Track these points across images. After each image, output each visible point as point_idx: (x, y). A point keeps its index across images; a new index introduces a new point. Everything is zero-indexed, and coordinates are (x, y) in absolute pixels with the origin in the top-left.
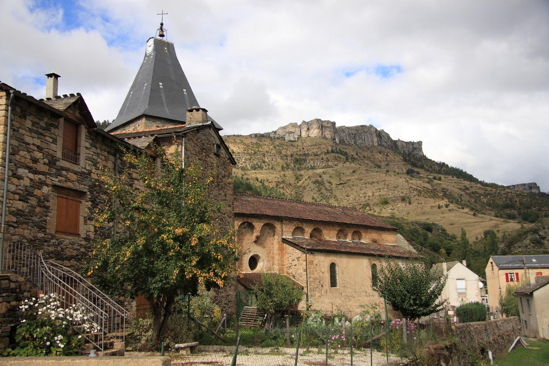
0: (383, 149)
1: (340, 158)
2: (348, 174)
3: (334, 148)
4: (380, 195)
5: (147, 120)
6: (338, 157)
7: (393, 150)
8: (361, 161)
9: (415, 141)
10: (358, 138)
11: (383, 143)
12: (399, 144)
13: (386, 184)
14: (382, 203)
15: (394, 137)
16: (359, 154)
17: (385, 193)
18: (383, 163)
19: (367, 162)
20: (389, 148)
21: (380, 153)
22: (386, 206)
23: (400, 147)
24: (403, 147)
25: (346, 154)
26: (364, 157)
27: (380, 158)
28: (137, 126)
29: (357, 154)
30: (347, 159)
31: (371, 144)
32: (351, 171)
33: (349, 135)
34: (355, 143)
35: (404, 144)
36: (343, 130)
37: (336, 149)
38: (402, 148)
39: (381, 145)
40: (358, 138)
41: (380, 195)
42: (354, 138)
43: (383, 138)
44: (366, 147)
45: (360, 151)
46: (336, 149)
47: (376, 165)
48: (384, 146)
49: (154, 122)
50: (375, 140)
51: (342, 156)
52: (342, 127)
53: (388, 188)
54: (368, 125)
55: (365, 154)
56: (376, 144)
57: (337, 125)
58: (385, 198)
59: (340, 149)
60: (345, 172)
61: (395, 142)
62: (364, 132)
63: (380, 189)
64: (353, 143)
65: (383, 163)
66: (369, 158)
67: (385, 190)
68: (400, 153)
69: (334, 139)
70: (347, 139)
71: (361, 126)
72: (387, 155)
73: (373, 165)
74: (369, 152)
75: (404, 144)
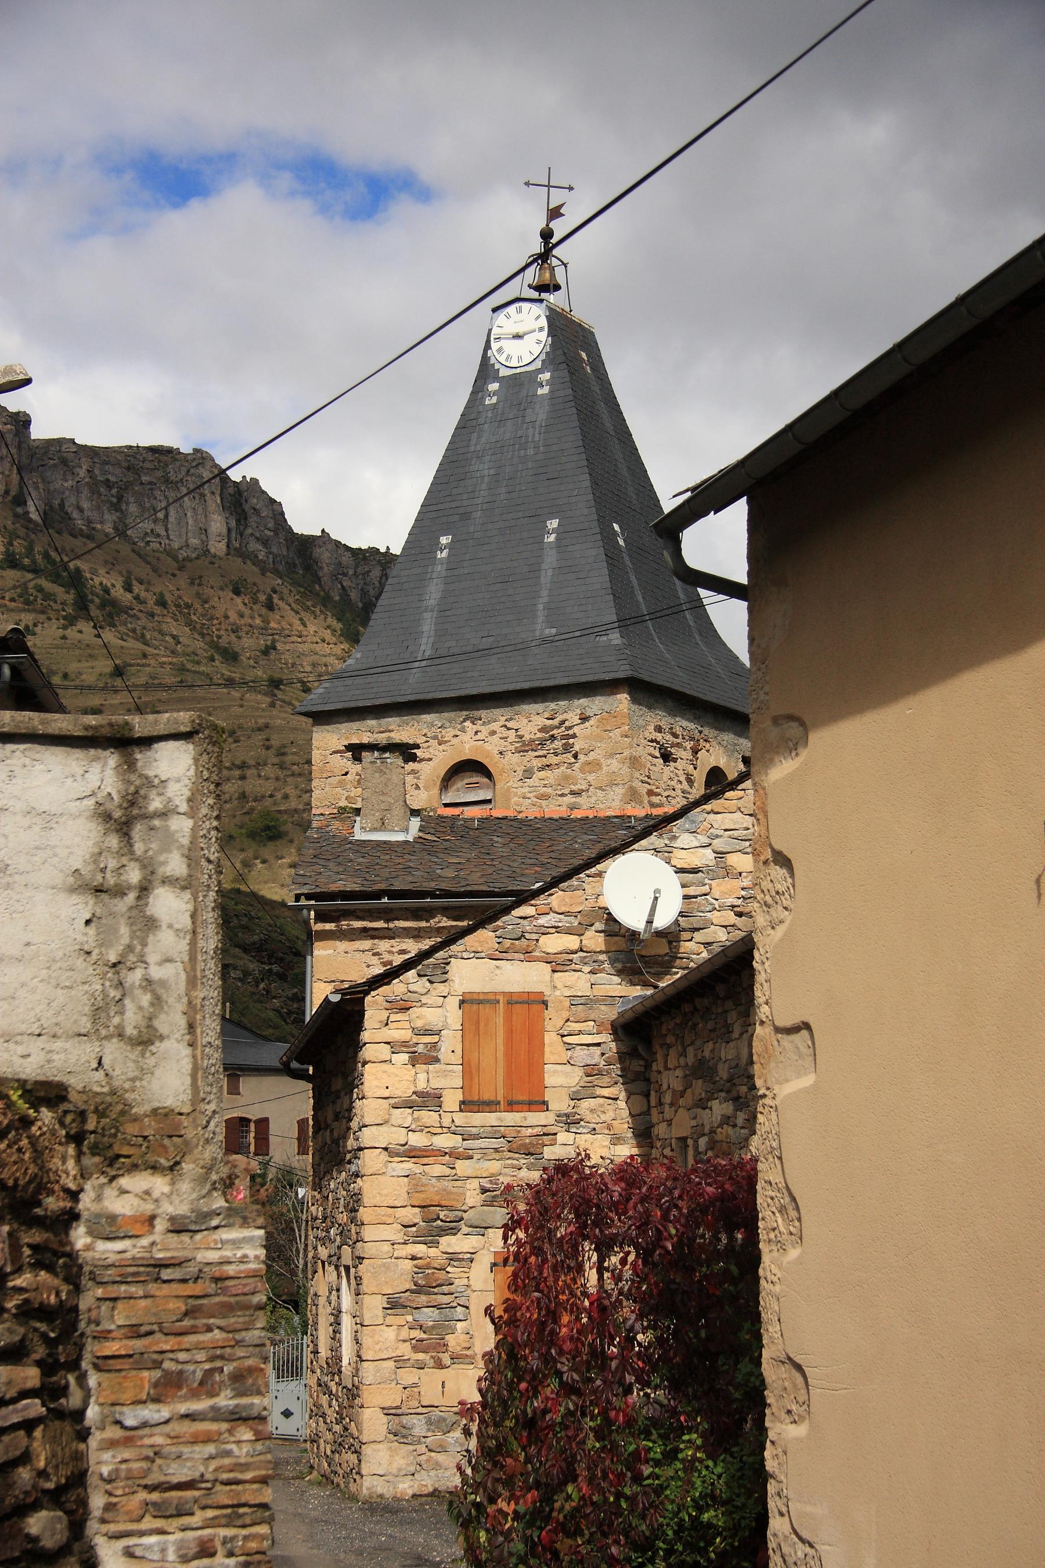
0: (251, 571)
1: (48, 596)
2: (89, 678)
3: (19, 546)
4: (243, 796)
5: (634, 700)
6: (40, 589)
7: (295, 583)
8: (144, 621)
9: (333, 537)
10: (133, 508)
11: (253, 546)
12: (324, 555)
13: (275, 742)
14: (252, 835)
15: (303, 521)
16: (137, 588)
17: (268, 787)
18: (247, 642)
19: (172, 627)
20: (277, 573)
21: (237, 592)
22: (267, 851)
23: (325, 572)
24: (339, 571)
25: (75, 581)
26: (162, 603)
27: (233, 616)
28: (573, 718)
29: (128, 588)
30: (82, 605)
31: (194, 541)
32: (105, 666)
33: (94, 487)
34: (121, 532)
35: (347, 559)
36: (64, 462)
37: (30, 549)
38: (334, 576)
39: (242, 554)
40: (133, 508)
41: (243, 796)
42: (116, 507)
43: (253, 520)
44: (171, 554)
45: (142, 570)
46: (30, 549)
47: (215, 646)
48: (253, 558)
49: (650, 707)
50: (218, 523)
51: (58, 590)
52: (60, 442)
53: (282, 766)
54: (186, 449)
55: (167, 587)
56: (218, 547)
57: (38, 432)
58: (266, 814)
59: (46, 556)
60: (73, 667)
61: (306, 545)
62: (167, 481)
63: (243, 766)
64: (109, 528)
65: (247, 642)
66: (183, 610)
67: (268, 771)
68: (326, 601)
69: (20, 500)
70: (83, 508)
71: (154, 450)
72: (270, 606)
73: (199, 644)
74: (183, 580)
75: (347, 559)
